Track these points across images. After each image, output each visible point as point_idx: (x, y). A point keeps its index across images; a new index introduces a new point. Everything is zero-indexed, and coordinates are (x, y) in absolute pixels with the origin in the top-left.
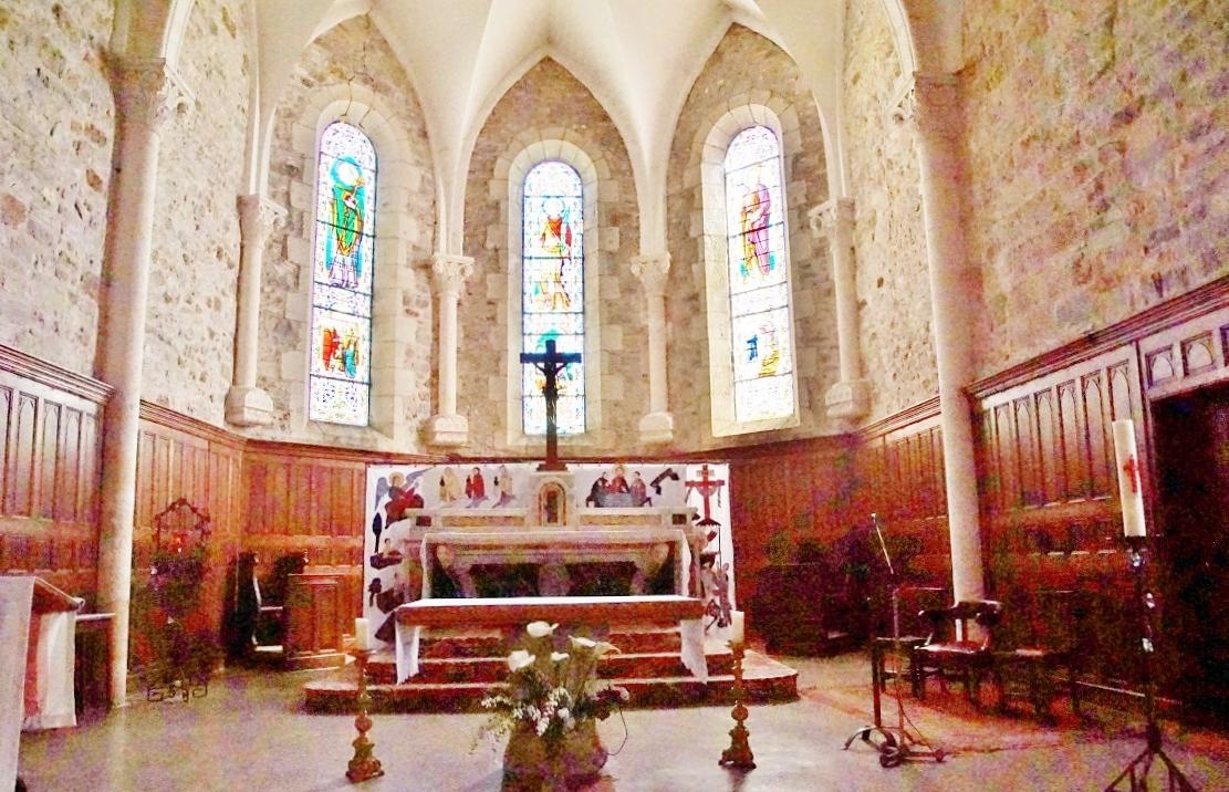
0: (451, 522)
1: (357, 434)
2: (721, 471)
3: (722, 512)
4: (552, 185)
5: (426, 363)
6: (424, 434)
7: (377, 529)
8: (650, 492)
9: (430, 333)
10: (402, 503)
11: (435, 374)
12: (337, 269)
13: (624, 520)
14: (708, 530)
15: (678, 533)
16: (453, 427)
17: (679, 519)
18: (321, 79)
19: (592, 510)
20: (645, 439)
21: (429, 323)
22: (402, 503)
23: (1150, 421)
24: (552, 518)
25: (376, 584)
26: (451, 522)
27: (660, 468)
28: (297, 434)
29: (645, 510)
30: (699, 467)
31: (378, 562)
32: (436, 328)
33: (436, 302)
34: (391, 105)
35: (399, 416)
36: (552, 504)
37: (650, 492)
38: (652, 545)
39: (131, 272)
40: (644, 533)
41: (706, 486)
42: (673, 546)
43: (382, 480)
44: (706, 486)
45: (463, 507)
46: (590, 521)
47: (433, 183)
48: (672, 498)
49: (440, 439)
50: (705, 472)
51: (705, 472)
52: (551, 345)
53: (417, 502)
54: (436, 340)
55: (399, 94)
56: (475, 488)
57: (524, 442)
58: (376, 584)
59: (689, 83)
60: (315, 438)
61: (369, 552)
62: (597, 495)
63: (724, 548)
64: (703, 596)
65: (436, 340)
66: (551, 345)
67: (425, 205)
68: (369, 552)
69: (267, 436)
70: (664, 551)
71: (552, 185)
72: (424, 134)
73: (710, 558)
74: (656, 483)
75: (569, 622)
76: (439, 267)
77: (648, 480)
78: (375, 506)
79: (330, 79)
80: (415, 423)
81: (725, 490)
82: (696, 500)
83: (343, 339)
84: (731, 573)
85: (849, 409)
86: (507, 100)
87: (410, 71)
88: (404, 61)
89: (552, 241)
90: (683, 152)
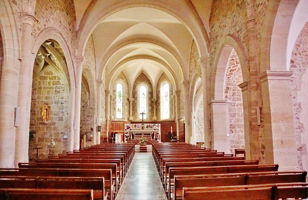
0: (133, 130)
1: (121, 119)
2: (160, 125)
3: (160, 129)
4: (143, 90)
5: (128, 111)
6: (128, 119)
7: (126, 130)
8: (152, 127)
9: (129, 107)
10: (128, 128)
11: (129, 112)
12: (119, 101)
13: (150, 129)
14: (158, 130)
15: (154, 131)
16: (131, 118)
17: (155, 129)
18: (117, 79)
19: (147, 129)
20: (153, 120)
21: (129, 106)
22: (128, 128)
23: (5, 170)
24: (143, 129)
25: (126, 136)
26: (133, 130)
27: (153, 124)
28: (115, 120)
29: (152, 129)
30: (157, 124)
31: (126, 133)
32: (129, 107)
33: (129, 104)
34: (124, 81)
35: (126, 117)
36: (143, 128)
37: (152, 127)
38: (152, 132)
39: (107, 109)
40: (151, 131)
41: (158, 126)
42: (154, 132)
43: (126, 126)
44: (158, 126)
45: (134, 128)
46: (146, 130)
47: (129, 89)
48: (154, 127)
49: (130, 120)
50: (158, 125)
51: (158, 125)
52: (143, 112)
53: (130, 128)
54: (129, 108)
55: (125, 79)
56: (135, 126)
57: (139, 120)
58: (126, 136)
59: (159, 77)
60: (118, 120)
61: (125, 132)
62: (147, 127)
63: (160, 132)
64: (157, 137)
65: (129, 108)
66: (143, 112)
67: (128, 92)
68: (125, 132)
69: (113, 120)
70: (153, 133)
71: (143, 90)
72: (128, 83)
73: (158, 133)
74: (153, 126)
75: (144, 137)
76: (130, 100)
77: (152, 126)
78: (126, 128)
79: (118, 79)
80: (127, 118)
81: (160, 127)
82: (157, 128)
83: (120, 109)
84: (160, 135)
85: (174, 118)
86: (137, 78)
87: (126, 76)
88: (126, 75)
89: (143, 95)
90: (158, 86)
